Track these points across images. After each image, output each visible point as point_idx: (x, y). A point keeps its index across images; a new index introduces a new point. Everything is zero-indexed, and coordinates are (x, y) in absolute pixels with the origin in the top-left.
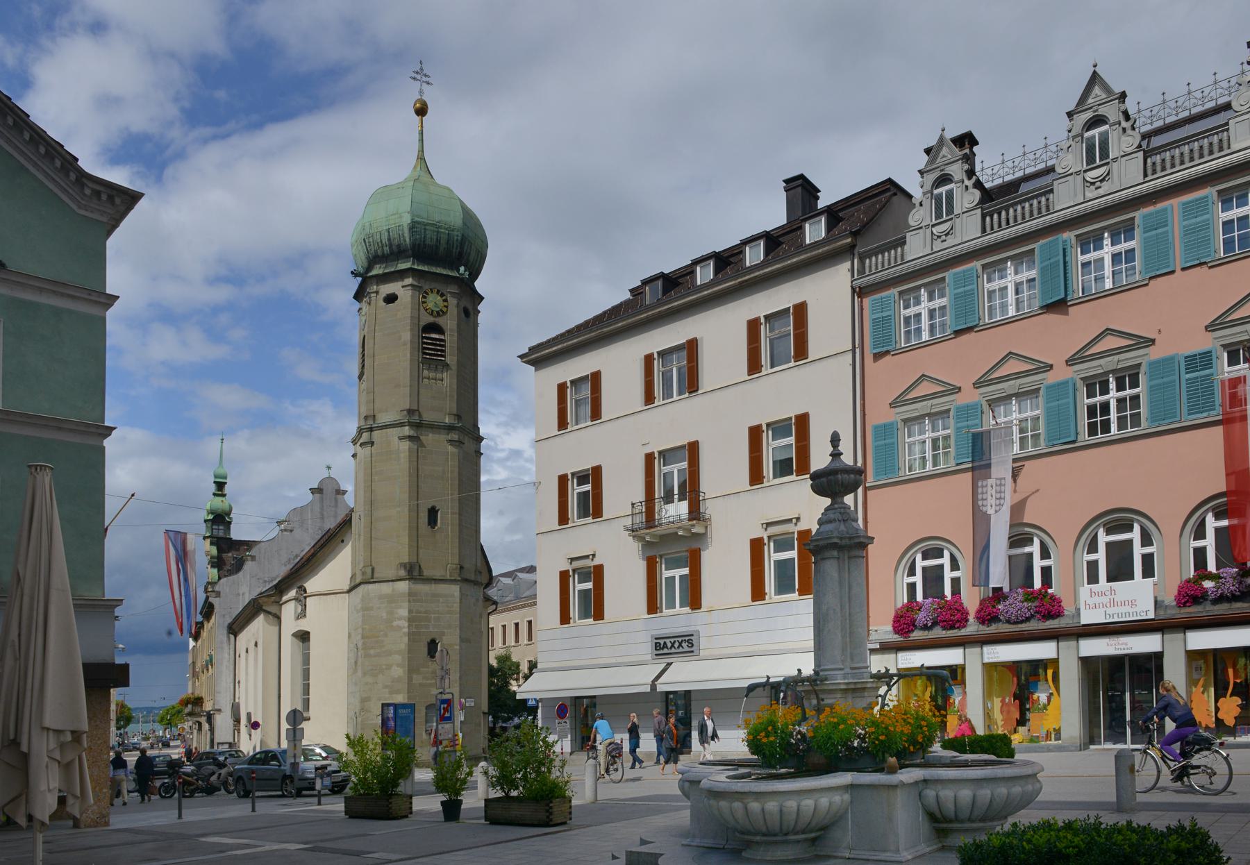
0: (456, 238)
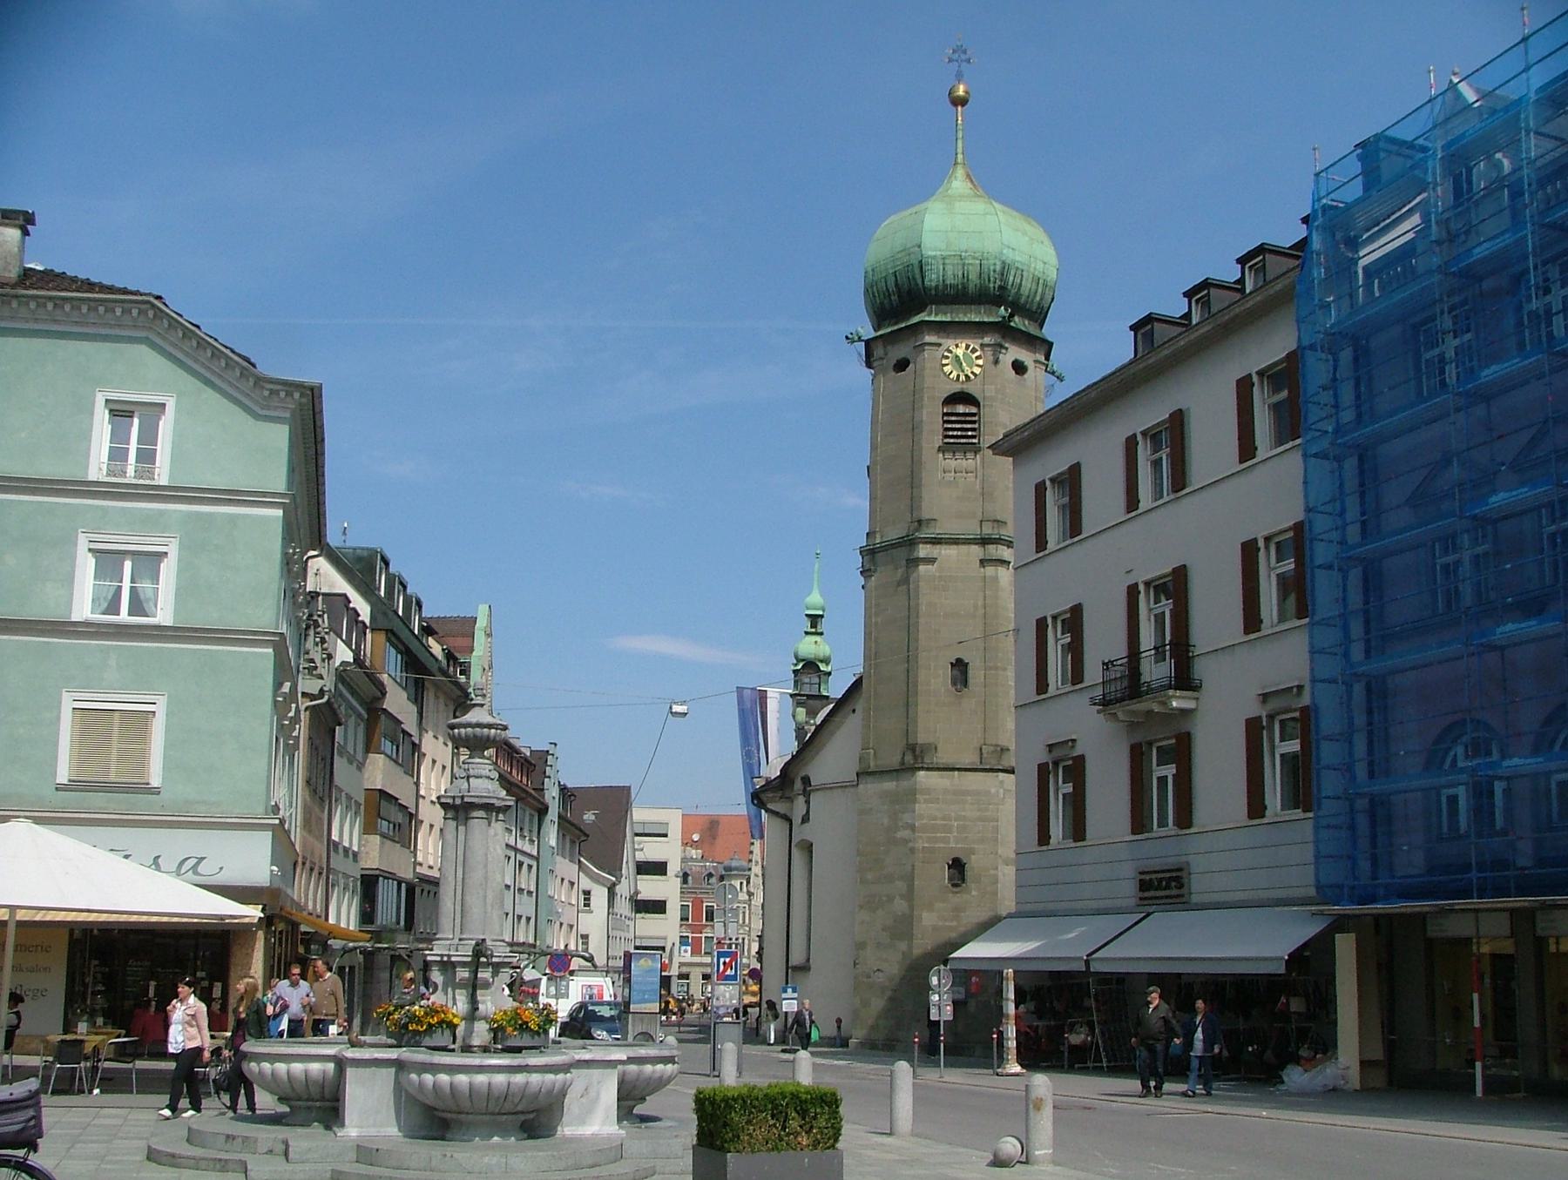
0: (992, 268)
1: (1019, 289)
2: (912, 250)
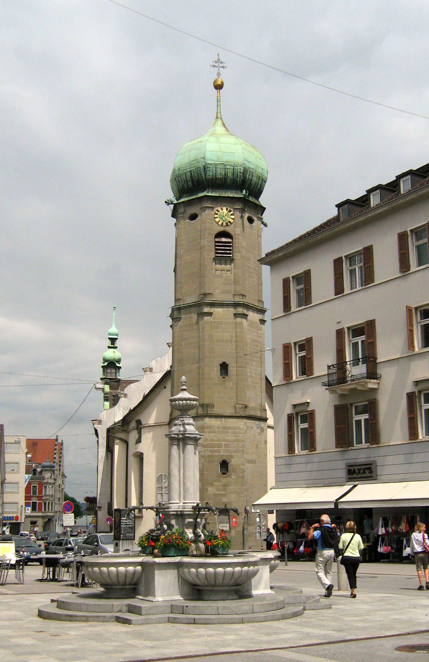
0: (239, 170)
1: (251, 181)
2: (200, 160)
